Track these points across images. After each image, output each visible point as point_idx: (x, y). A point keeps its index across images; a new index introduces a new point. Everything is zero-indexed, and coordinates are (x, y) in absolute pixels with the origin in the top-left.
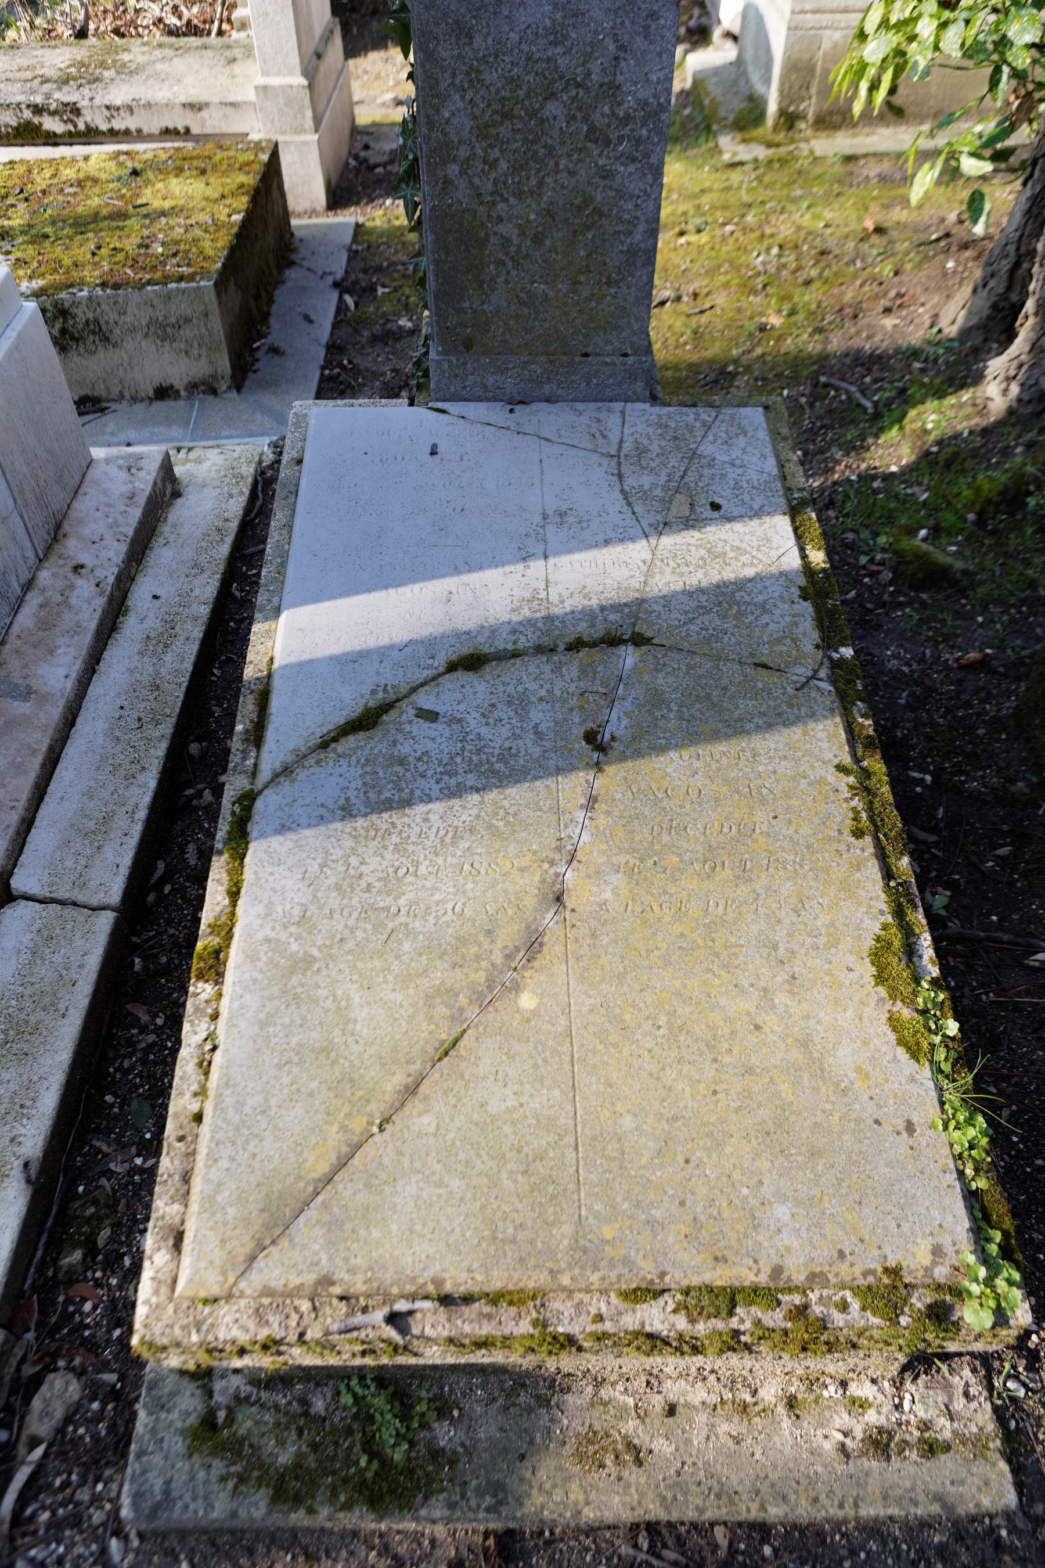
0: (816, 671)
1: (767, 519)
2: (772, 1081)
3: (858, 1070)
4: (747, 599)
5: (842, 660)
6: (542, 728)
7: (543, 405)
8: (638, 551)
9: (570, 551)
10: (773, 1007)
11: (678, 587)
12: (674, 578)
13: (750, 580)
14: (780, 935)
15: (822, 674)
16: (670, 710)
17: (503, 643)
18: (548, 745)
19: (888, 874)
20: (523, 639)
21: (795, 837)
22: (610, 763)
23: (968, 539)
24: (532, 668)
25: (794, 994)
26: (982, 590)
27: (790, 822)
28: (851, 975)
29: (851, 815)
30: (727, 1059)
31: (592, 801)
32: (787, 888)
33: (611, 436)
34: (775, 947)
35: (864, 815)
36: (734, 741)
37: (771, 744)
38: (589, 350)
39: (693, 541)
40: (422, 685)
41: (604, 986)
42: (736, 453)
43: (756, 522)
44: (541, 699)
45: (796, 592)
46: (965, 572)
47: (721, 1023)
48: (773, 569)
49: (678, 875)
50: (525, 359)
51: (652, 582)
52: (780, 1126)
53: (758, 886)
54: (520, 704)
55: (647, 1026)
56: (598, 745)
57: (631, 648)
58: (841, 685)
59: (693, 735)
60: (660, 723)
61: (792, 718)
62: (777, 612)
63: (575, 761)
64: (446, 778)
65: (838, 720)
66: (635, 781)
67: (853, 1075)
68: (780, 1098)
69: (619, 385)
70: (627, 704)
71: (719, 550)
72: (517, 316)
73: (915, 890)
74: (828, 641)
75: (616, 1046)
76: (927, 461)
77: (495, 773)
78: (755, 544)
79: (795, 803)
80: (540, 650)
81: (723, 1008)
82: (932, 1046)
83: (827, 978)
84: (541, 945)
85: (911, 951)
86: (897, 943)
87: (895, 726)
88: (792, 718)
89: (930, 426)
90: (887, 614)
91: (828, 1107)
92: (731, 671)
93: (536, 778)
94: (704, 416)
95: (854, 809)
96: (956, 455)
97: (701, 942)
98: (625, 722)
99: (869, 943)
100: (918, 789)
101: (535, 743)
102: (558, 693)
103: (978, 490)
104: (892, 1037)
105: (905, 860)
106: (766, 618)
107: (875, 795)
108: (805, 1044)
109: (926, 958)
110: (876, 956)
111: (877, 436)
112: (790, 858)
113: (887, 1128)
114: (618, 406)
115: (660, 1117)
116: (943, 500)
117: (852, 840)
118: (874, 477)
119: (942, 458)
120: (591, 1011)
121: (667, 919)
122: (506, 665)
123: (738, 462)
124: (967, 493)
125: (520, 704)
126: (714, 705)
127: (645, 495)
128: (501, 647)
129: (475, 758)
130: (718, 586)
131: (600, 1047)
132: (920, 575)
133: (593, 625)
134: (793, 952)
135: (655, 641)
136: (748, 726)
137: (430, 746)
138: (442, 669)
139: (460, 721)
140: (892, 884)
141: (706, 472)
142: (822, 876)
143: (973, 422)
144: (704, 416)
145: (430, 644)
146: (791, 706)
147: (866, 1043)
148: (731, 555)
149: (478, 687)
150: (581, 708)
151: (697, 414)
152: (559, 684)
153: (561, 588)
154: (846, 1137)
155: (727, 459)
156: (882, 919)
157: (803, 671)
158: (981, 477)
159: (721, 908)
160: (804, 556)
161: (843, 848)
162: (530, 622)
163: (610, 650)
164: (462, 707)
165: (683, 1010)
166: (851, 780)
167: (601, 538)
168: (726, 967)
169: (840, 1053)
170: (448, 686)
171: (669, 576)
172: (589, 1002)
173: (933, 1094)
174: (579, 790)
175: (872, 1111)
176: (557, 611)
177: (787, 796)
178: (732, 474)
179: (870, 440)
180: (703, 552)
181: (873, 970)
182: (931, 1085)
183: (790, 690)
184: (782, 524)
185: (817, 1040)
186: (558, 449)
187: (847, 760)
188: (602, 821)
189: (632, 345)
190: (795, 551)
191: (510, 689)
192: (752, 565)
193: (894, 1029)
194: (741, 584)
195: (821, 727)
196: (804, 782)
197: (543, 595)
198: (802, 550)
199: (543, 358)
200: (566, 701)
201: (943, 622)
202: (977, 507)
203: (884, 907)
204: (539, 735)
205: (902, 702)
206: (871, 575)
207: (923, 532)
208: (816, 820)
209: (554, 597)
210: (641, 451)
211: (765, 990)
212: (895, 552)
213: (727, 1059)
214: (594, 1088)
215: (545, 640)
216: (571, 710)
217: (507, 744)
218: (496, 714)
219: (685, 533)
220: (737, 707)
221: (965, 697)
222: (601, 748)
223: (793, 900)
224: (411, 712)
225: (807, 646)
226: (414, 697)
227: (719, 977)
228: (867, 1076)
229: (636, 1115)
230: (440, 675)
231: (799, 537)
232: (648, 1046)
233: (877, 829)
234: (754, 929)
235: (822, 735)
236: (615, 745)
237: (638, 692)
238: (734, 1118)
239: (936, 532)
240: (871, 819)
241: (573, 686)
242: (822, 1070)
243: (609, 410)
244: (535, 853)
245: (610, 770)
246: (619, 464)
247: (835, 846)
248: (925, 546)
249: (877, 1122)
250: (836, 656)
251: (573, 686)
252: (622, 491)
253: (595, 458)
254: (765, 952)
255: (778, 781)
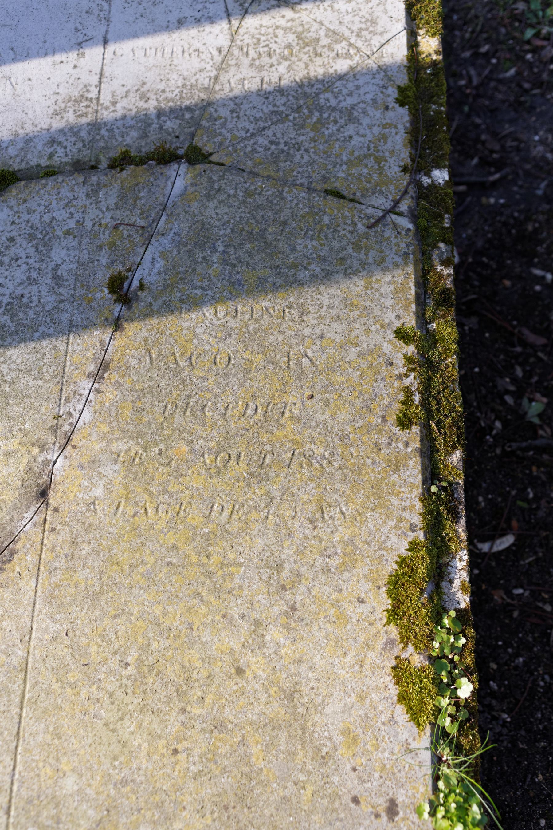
0: (396, 203)
2: (243, 742)
3: (346, 732)
4: (333, 102)
5: (434, 186)
6: (63, 271)
8: (216, 35)
9: (135, 35)
10: (262, 645)
11: (253, 85)
12: (252, 73)
13: (341, 77)
14: (288, 553)
15: (404, 207)
16: (214, 250)
18: (65, 292)
19: (431, 474)
20: (60, 152)
21: (330, 423)
22: (132, 320)
24: (65, 192)
25: (289, 630)
27: (327, 404)
28: (361, 608)
29: (401, 397)
30: (197, 711)
31: (103, 366)
32: (307, 492)
34: (279, 568)
35: (417, 398)
36: (281, 294)
39: (282, 22)
41: (74, 609)
44: (68, 233)
45: (392, 92)
47: (198, 664)
48: (371, 63)
49: (183, 468)
51: (223, 78)
52: (242, 799)
53: (274, 488)
55: (114, 662)
56: (124, 296)
57: (184, 167)
58: (422, 221)
59: (236, 286)
61: (356, 264)
62: (366, 121)
63: (92, 315)
65: (410, 269)
66: (157, 344)
67: (338, 738)
68: (249, 764)
70: (166, 241)
71: (312, 35)
73: (461, 494)
74: (419, 164)
75: (73, 686)
78: (355, 28)
79: (338, 378)
80: (80, 167)
81: (204, 644)
82: (438, 710)
83: (332, 611)
84: (12, 553)
85: (439, 574)
86: (422, 571)
87: (528, 219)
88: (356, 264)
90: (543, 95)
91: (302, 777)
92: (295, 198)
93: (45, 336)
95: (407, 390)
97: (194, 558)
98: (160, 264)
99: (390, 566)
100: (538, 288)
101: (52, 292)
104: (394, 691)
105: (457, 456)
106: (350, 130)
107: (436, 369)
108: (291, 695)
109: (457, 583)
110: (396, 585)
112: (318, 451)
113: (365, 808)
115: (107, 778)
117: (396, 430)
120: (54, 639)
121: (161, 525)
125: (42, 238)
126: (267, 245)
128: (33, 163)
130: (301, 85)
131: (56, 686)
133: (145, 135)
134: (299, 576)
136: (303, 275)
140: (434, 489)
142: (352, 476)
146: (357, 248)
147: (361, 698)
148: (325, 41)
152: (93, 213)
153: (116, 85)
154: (315, 818)
156: (412, 536)
157: (383, 202)
159: (226, 514)
160: (413, 44)
161: (384, 440)
162: (73, 131)
165: (158, 645)
166: (411, 349)
167: (173, 17)
168: (217, 590)
169: (328, 710)
171: (246, 72)
172: (54, 627)
173: (428, 770)
174: (90, 354)
175: (352, 785)
176: (107, 115)
177: (330, 370)
180: (291, 38)
181: (388, 603)
182: (427, 756)
185: (305, 690)
187: (410, 321)
188: (111, 394)
190: (403, 38)
191: (35, 219)
192: (348, 55)
193: (398, 681)
194: (328, 83)
195: (388, 278)
196: (354, 350)
197: (93, 94)
198: (412, 35)
200: (96, 235)
203: (417, 520)
204: (57, 279)
205: (540, 192)
206: (535, 51)
208: (359, 403)
211: (257, 623)
213: (197, 711)
214: (40, 738)
215: (86, 155)
216: (100, 248)
217: (18, 292)
219: (275, 12)
220: (294, 249)
222: (125, 299)
223: (311, 508)
225: (393, 169)
227: (207, 603)
228: (355, 740)
229: (81, 775)
232: (110, 688)
233: (430, 415)
234: (259, 542)
235: (387, 289)
237: (181, 226)
238: (191, 785)
240: (425, 403)
241: (108, 215)
242: (304, 730)
244: (26, 433)
245: (131, 328)
247: (374, 437)
249: (356, 800)
250: (426, 181)
251: (108, 215)
254: (266, 573)
255: (323, 349)
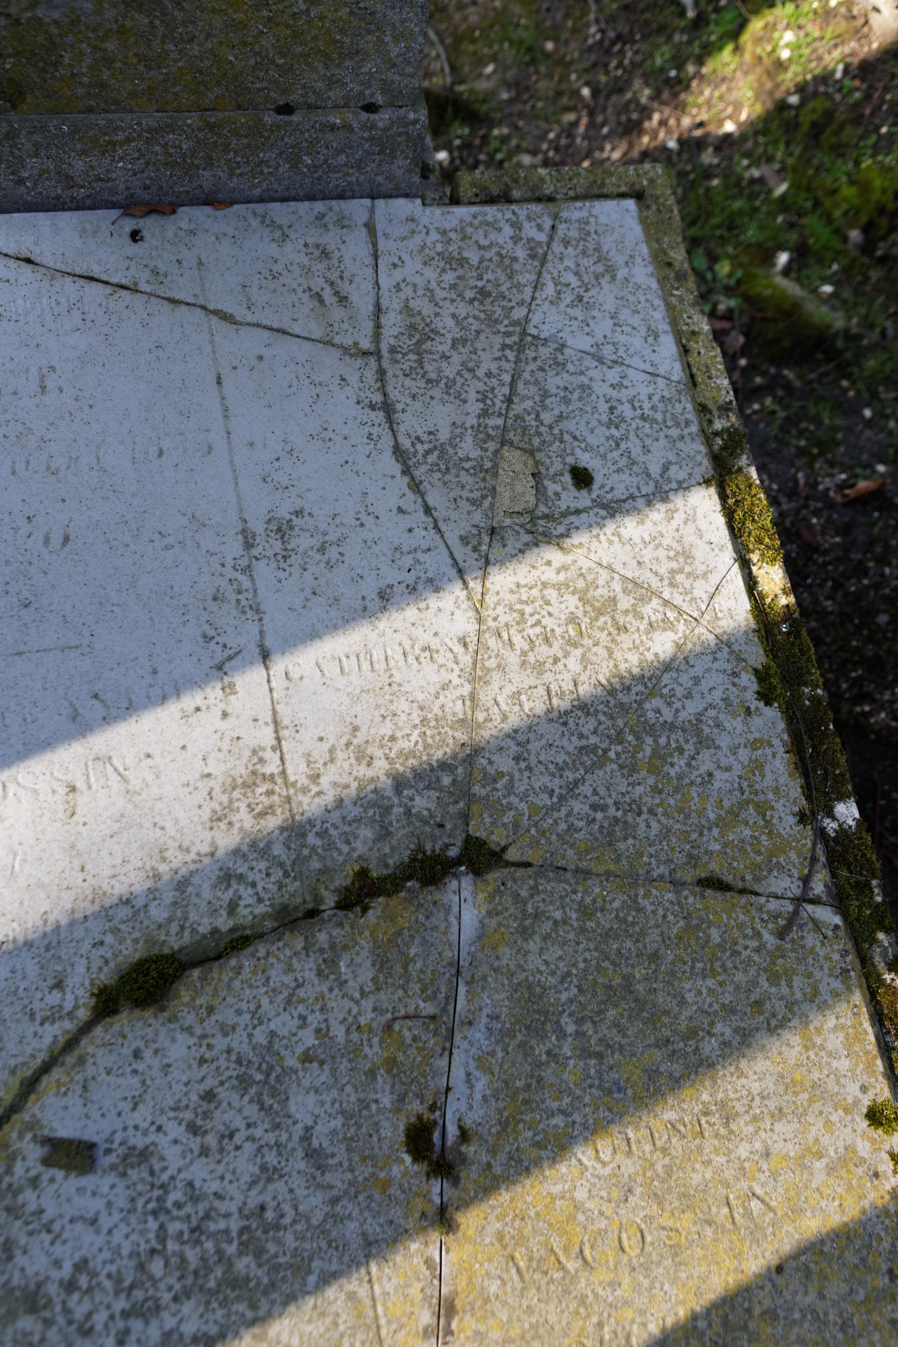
0: (806, 880)
1: (678, 501)
4: (667, 714)
7: (201, 214)
8: (446, 614)
9: (314, 635)
11: (536, 704)
13: (667, 667)
16: (562, 1034)
17: (207, 920)
18: (337, 1179)
21: (820, 1306)
23: (846, 270)
24: (277, 975)
26: (871, 363)
33: (354, 298)
36: (686, 1093)
37: (754, 1077)
38: (294, 98)
39: (549, 574)
40: (46, 1068)
42: (603, 327)
43: (657, 514)
44: (307, 1058)
45: (748, 681)
46: (847, 334)
50: (150, 120)
54: (264, 1078)
60: (548, 1074)
62: (724, 741)
63: (396, 1213)
64: (136, 1325)
69: (359, 166)
70: (478, 1034)
72: (122, 31)
76: (779, 121)
77: (237, 1283)
88: (781, 1010)
89: (785, 54)
93: (327, 1279)
94: (530, 231)
96: (829, 115)
98: (481, 1084)
102: (338, 1031)
103: (865, 188)
111: (700, 61)
114: (358, 208)
116: (811, 197)
118: (700, 144)
119: (806, 120)
122: (221, 973)
123: (607, 352)
124: (848, 192)
127: (444, 456)
128: (204, 928)
129: (192, 1255)
130: (612, 692)
132: (786, 343)
133: (385, 833)
135: (512, 855)
136: (710, 1046)
137: (90, 1242)
138: (83, 1014)
139: (144, 1155)
141: (553, 382)
143: (847, 49)
144: (530, 231)
145: (47, 947)
148: (625, 602)
149: (167, 1050)
150: (391, 1064)
151: (516, 225)
155: (585, 343)
158: (866, 163)
162: (257, 848)
163: (428, 895)
164: (143, 1116)
167: (370, 587)
170: (104, 1059)
171: (520, 679)
174: (415, 1291)
176: (309, 805)
178: (601, 381)
179: (691, 69)
180: (572, 601)
183: (770, 940)
184: (705, 504)
186: (251, 342)
189: (386, 87)
191: (239, 1042)
192: (667, 625)
194: (652, 681)
197: (272, 768)
199: (193, 119)
201: (818, 422)
202: (864, 218)
207: (783, 258)
209: (297, 771)
210: (421, 334)
212: (747, 298)
215: (295, 892)
216: (372, 1074)
217: (254, 1201)
218: (221, 1118)
219: (532, 556)
220: (682, 1002)
221: (856, 556)
222: (443, 1167)
224: (33, 1152)
225: (786, 822)
226: (32, 1109)
230: (86, 1028)
231: (735, 531)
235: (835, 1042)
236: (469, 1150)
237: (494, 999)
239: (803, 255)
241: (367, 1005)
243: (343, 223)
245: (469, 1220)
246: (381, 373)
248: (791, 288)
251: (367, 1005)
252: (398, 451)
253: (330, 358)
255: (775, 1175)
